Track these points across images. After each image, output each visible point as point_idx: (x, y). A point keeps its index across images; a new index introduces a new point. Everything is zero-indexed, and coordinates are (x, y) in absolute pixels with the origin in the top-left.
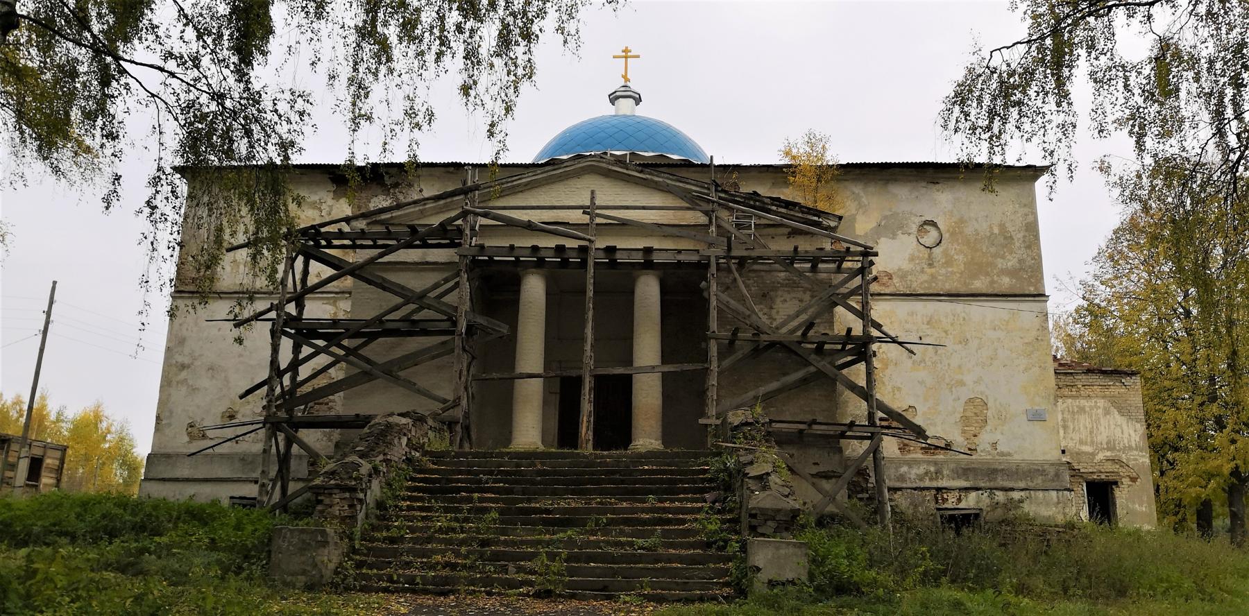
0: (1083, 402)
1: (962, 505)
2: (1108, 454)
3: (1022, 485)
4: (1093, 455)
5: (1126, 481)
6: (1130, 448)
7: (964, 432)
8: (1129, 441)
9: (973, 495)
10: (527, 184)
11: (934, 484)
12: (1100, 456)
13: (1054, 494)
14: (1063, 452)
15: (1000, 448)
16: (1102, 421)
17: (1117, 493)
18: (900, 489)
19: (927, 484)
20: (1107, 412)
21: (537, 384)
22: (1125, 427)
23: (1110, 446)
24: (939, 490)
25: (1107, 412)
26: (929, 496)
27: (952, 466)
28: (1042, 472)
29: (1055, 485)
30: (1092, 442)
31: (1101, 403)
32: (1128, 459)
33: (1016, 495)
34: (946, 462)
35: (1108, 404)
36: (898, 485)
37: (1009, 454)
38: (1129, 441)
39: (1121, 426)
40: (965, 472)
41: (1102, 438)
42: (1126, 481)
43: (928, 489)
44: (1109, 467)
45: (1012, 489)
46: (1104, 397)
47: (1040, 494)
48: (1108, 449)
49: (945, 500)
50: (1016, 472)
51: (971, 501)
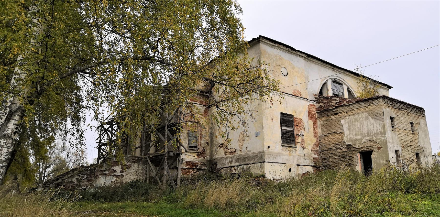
0: (357, 116)
2: (368, 138)
3: (252, 162)
4: (361, 139)
5: (376, 150)
6: (378, 133)
7: (239, 145)
8: (377, 130)
10: (272, 45)
11: (231, 165)
12: (364, 140)
13: (259, 164)
15: (248, 149)
16: (365, 123)
17: (372, 156)
19: (230, 165)
20: (367, 119)
22: (375, 124)
23: (369, 134)
24: (231, 167)
25: (367, 119)
27: (235, 158)
28: (257, 156)
30: (361, 134)
31: (364, 115)
33: (249, 166)
34: (234, 157)
35: (367, 115)
36: (223, 166)
37: (250, 151)
38: (377, 130)
39: (373, 124)
40: (238, 160)
41: (365, 131)
42: (376, 150)
43: (229, 167)
44: (369, 144)
46: (365, 112)
47: (256, 164)
48: (368, 136)
49: (232, 170)
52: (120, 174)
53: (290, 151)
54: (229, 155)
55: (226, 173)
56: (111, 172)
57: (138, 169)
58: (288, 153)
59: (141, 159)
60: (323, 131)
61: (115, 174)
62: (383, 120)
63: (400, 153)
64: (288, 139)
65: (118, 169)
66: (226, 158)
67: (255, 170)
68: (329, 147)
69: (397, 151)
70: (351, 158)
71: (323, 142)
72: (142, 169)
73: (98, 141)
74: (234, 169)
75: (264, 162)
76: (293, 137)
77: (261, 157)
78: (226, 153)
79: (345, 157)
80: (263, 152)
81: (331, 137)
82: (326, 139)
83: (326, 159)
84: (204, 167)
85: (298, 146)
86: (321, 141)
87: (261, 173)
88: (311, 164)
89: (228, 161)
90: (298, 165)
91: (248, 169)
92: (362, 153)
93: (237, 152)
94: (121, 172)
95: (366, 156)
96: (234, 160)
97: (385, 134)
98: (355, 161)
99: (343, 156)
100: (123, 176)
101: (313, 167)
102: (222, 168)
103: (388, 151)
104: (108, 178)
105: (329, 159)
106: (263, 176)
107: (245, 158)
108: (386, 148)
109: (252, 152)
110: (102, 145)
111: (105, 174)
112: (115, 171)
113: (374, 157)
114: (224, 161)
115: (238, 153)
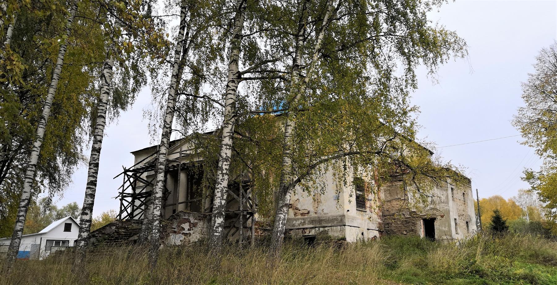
1: (310, 234)
3: (330, 225)
5: (439, 217)
7: (313, 207)
9: (313, 230)
11: (303, 227)
14: (348, 211)
15: (325, 211)
17: (435, 223)
18: (292, 230)
19: (301, 227)
21: (180, 201)
24: (304, 229)
26: (300, 231)
28: (336, 219)
29: (341, 224)
32: (440, 208)
33: (326, 229)
34: (307, 218)
36: (293, 228)
40: (312, 221)
42: (439, 217)
44: (431, 212)
45: (326, 227)
47: (335, 228)
49: (305, 232)
50: (328, 220)
51: (313, 232)
52: (188, 232)
53: (362, 215)
54: (300, 217)
55: (296, 235)
56: (181, 230)
57: (203, 228)
58: (360, 217)
59: (206, 217)
60: (386, 196)
61: (184, 232)
62: (447, 190)
63: (458, 221)
64: (361, 203)
65: (186, 226)
66: (296, 220)
67: (334, 233)
68: (392, 212)
69: (455, 219)
70: (414, 224)
71: (386, 207)
72: (207, 228)
73: (121, 191)
74: (307, 231)
75: (345, 225)
76: (364, 202)
77: (341, 220)
78: (295, 214)
79: (408, 223)
80: (344, 216)
81: (394, 203)
82: (389, 204)
83: (388, 224)
84: (269, 228)
85: (368, 210)
86: (384, 206)
87: (341, 236)
88: (377, 229)
89: (299, 222)
90: (368, 229)
91: (326, 232)
92: (425, 220)
93: (310, 214)
94: (189, 230)
95: (429, 224)
96: (306, 222)
97: (448, 204)
98: (418, 228)
99: (406, 222)
100: (190, 234)
101: (379, 231)
102: (291, 230)
103: (450, 219)
104: (178, 236)
105: (391, 224)
106: (344, 239)
107: (322, 220)
108: (449, 216)
109: (330, 214)
110: (125, 196)
111: (175, 232)
112: (184, 229)
113: (437, 224)
114: (295, 222)
115: (312, 215)
